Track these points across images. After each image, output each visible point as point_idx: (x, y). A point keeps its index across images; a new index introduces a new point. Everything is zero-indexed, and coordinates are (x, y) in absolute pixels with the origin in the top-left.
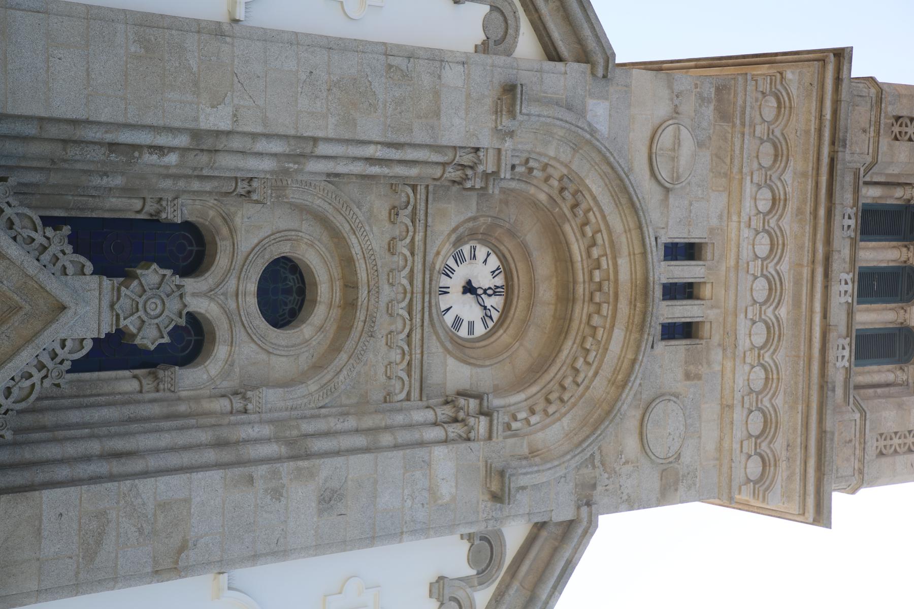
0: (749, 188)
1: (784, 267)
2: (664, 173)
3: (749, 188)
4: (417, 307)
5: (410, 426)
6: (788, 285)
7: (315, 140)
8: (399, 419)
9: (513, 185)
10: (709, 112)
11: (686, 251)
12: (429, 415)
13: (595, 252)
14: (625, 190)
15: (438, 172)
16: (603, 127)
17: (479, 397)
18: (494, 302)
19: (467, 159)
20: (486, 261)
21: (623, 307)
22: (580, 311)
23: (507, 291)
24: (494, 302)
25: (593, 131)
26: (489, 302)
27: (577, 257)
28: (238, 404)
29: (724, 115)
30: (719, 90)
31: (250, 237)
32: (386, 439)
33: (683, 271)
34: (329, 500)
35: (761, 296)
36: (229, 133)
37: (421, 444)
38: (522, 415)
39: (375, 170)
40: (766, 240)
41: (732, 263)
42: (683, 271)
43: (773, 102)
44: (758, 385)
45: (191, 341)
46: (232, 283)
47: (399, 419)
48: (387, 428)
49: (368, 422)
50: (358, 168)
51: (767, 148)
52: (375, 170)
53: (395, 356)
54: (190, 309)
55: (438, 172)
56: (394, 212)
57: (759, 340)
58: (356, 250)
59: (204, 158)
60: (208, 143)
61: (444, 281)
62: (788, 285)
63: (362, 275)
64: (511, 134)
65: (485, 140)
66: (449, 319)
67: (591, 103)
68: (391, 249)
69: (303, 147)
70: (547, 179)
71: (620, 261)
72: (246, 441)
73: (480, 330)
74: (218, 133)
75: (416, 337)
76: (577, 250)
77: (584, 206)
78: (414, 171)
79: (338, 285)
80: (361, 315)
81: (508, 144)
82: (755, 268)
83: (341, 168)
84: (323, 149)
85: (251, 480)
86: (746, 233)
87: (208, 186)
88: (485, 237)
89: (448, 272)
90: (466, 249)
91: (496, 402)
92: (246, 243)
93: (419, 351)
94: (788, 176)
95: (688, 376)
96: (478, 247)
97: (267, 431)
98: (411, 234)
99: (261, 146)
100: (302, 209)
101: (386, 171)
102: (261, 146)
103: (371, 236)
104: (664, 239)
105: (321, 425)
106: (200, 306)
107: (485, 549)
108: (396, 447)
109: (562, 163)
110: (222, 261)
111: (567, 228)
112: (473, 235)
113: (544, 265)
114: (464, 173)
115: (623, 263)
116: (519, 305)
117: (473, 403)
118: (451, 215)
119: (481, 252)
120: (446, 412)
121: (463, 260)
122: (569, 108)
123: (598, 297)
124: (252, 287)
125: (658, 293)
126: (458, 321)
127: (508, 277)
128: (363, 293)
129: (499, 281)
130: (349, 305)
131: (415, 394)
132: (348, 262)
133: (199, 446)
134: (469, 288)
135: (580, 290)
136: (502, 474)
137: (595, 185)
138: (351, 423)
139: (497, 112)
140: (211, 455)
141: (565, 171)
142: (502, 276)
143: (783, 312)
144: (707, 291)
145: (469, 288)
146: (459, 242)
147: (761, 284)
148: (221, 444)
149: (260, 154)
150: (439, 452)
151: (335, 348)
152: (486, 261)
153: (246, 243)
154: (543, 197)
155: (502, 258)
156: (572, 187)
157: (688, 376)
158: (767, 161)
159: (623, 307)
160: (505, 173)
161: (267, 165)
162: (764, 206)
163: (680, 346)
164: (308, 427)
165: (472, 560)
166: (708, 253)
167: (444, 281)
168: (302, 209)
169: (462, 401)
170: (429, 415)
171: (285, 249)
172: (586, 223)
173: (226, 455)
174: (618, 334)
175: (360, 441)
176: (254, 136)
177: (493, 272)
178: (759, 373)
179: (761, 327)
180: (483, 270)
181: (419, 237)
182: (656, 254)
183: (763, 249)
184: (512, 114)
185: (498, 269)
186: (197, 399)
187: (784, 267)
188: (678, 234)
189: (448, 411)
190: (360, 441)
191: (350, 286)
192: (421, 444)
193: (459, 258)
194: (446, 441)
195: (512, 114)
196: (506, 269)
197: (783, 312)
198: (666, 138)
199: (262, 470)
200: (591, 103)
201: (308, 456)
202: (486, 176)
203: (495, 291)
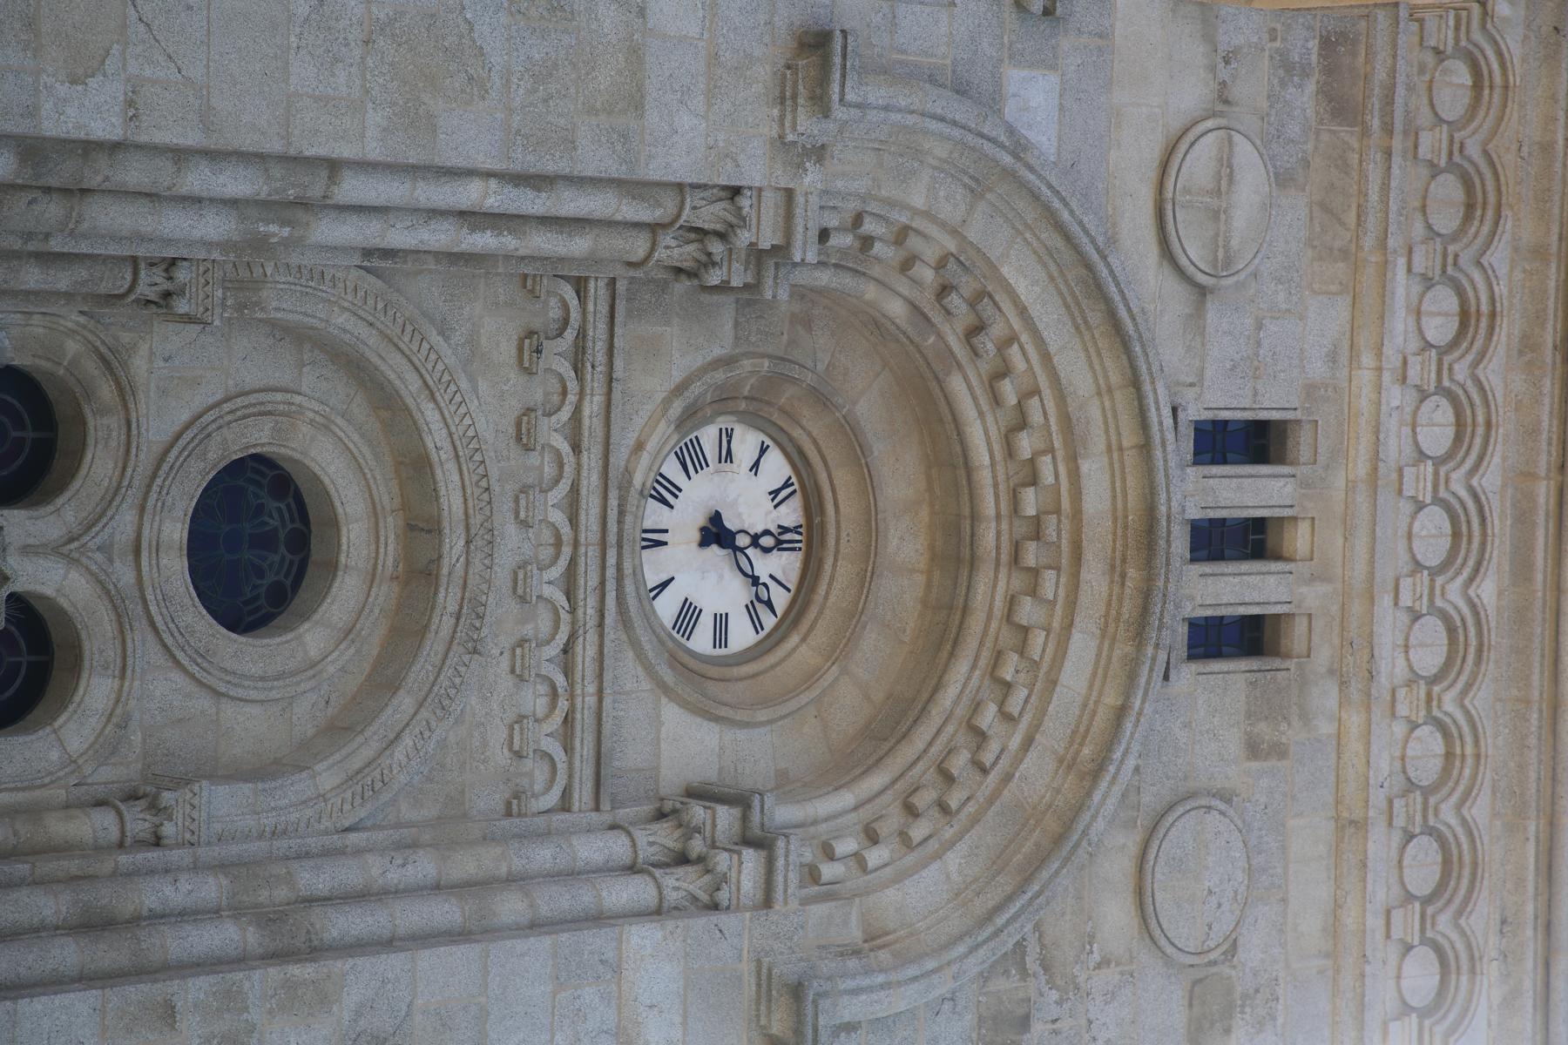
0: (1402, 286)
1: (1491, 480)
2: (1194, 251)
3: (1402, 286)
4: (588, 579)
5: (570, 875)
6: (1500, 524)
7: (334, 167)
8: (543, 856)
9: (824, 278)
10: (1305, 98)
11: (1248, 441)
12: (617, 847)
13: (1026, 444)
14: (1097, 290)
15: (638, 246)
16: (1043, 136)
17: (741, 801)
18: (779, 566)
19: (710, 214)
20: (756, 465)
21: (1095, 578)
22: (990, 588)
23: (809, 538)
24: (779, 566)
25: (1019, 148)
26: (765, 566)
27: (981, 454)
28: (138, 822)
29: (1341, 105)
30: (1328, 44)
31: (173, 403)
32: (511, 907)
33: (1242, 491)
35: (1433, 550)
36: (115, 147)
37: (598, 918)
38: (845, 846)
39: (484, 241)
40: (1445, 414)
41: (1362, 470)
42: (1242, 491)
43: (1463, 76)
44: (1427, 769)
46: (125, 520)
47: (543, 856)
48: (513, 880)
49: (467, 865)
50: (439, 236)
51: (1449, 188)
52: (484, 241)
53: (534, 699)
54: (19, 586)
55: (638, 246)
56: (531, 344)
57: (1429, 659)
58: (436, 438)
59: (53, 210)
60: (64, 172)
61: (655, 515)
62: (1500, 524)
63: (452, 502)
64: (819, 153)
65: (755, 169)
66: (667, 607)
67: (1014, 77)
68: (523, 438)
69: (303, 184)
70: (906, 265)
71: (1085, 466)
72: (157, 917)
73: (742, 635)
74: (89, 148)
75: (586, 652)
76: (981, 437)
77: (997, 330)
78: (579, 245)
79: (391, 526)
80: (448, 598)
81: (812, 178)
82: (1419, 481)
83: (399, 236)
84: (353, 188)
85: (168, 1014)
86: (1395, 396)
87: (63, 280)
88: (759, 406)
89: (664, 493)
90: (708, 437)
91: (784, 813)
92: (159, 421)
93: (591, 689)
94: (1499, 257)
95: (1254, 749)
96: (739, 431)
97: (210, 889)
98: (572, 398)
99: (198, 179)
100: (299, 337)
101: (509, 242)
102: (198, 179)
103: (473, 406)
104: (1194, 412)
105: (347, 874)
106: (43, 578)
108: (535, 926)
109: (943, 225)
110: (98, 466)
111: (956, 384)
112: (724, 401)
113: (900, 475)
114: (703, 250)
115: (1094, 470)
116: (840, 574)
117: (726, 817)
118: (672, 354)
119: (746, 442)
120: (657, 839)
121: (701, 463)
122: (962, 90)
123: (1032, 555)
124: (176, 532)
125: (1180, 543)
126: (688, 614)
128: (454, 546)
129: (790, 514)
130: (420, 574)
131: (583, 794)
132: (416, 468)
133: (37, 931)
134: (716, 533)
135: (988, 537)
136: (796, 992)
137: (1025, 279)
138: (424, 867)
139: (784, 99)
140: (67, 954)
141: (951, 245)
142: (796, 501)
143: (1487, 591)
144: (1299, 539)
145: (716, 533)
146: (691, 418)
147: (1434, 523)
148: (92, 925)
149: (195, 201)
150: (642, 938)
151: (384, 680)
152: (756, 465)
153: (159, 421)
154: (896, 308)
155: (797, 457)
156: (967, 285)
157: (1254, 749)
158: (1446, 221)
159: (1095, 578)
160: (805, 250)
161: (214, 226)
162: (1440, 329)
163: (1232, 677)
164: (314, 879)
166: (1302, 445)
167: (655, 515)
168: (299, 337)
169: (698, 812)
170: (617, 847)
171: (258, 437)
172: (1003, 372)
173: (108, 953)
174: (1083, 647)
175: (445, 912)
176: (180, 155)
177: (776, 493)
178: (1429, 743)
179: (1432, 629)
180: (751, 490)
181: (592, 406)
182: (1175, 448)
183: (1437, 432)
184: (821, 103)
185: (787, 485)
186: (34, 812)
187: (1491, 480)
188: (1228, 398)
189: (665, 836)
190: (445, 912)
191: (422, 526)
192: (598, 918)
193: (692, 459)
194: (658, 912)
195: (821, 103)
196: (805, 485)
197: (1487, 591)
198: (1199, 163)
199: (198, 988)
200: (1014, 77)
201: (315, 951)
202: (757, 256)
203: (780, 540)
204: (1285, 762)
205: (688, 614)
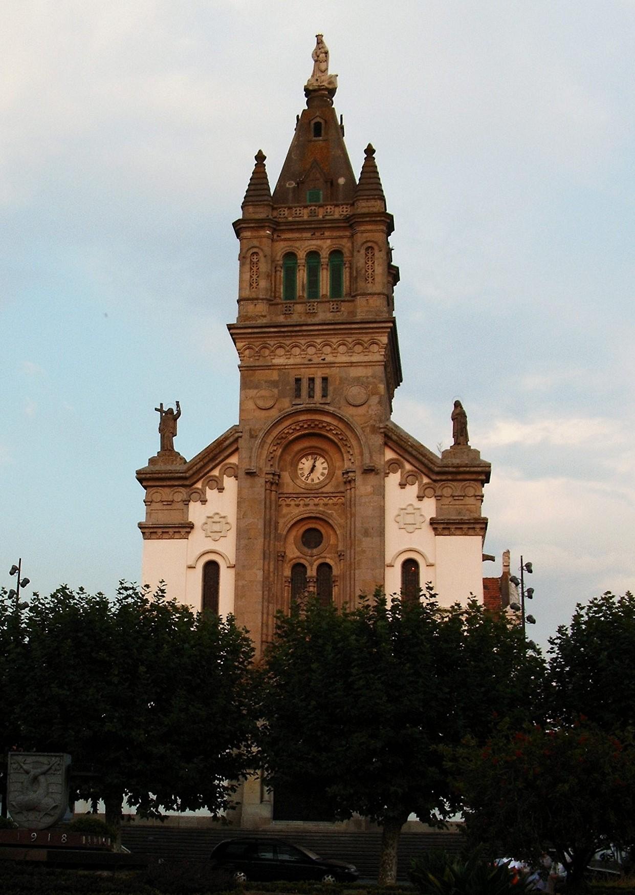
34: (366, 533)
45: (325, 568)
107: (394, 466)
118: (288, 484)
119: (300, 466)
126: (323, 474)
127: (309, 454)
129: (310, 457)
155: (302, 458)
165: (395, 472)
204: (328, 561)
205: (323, 474)
